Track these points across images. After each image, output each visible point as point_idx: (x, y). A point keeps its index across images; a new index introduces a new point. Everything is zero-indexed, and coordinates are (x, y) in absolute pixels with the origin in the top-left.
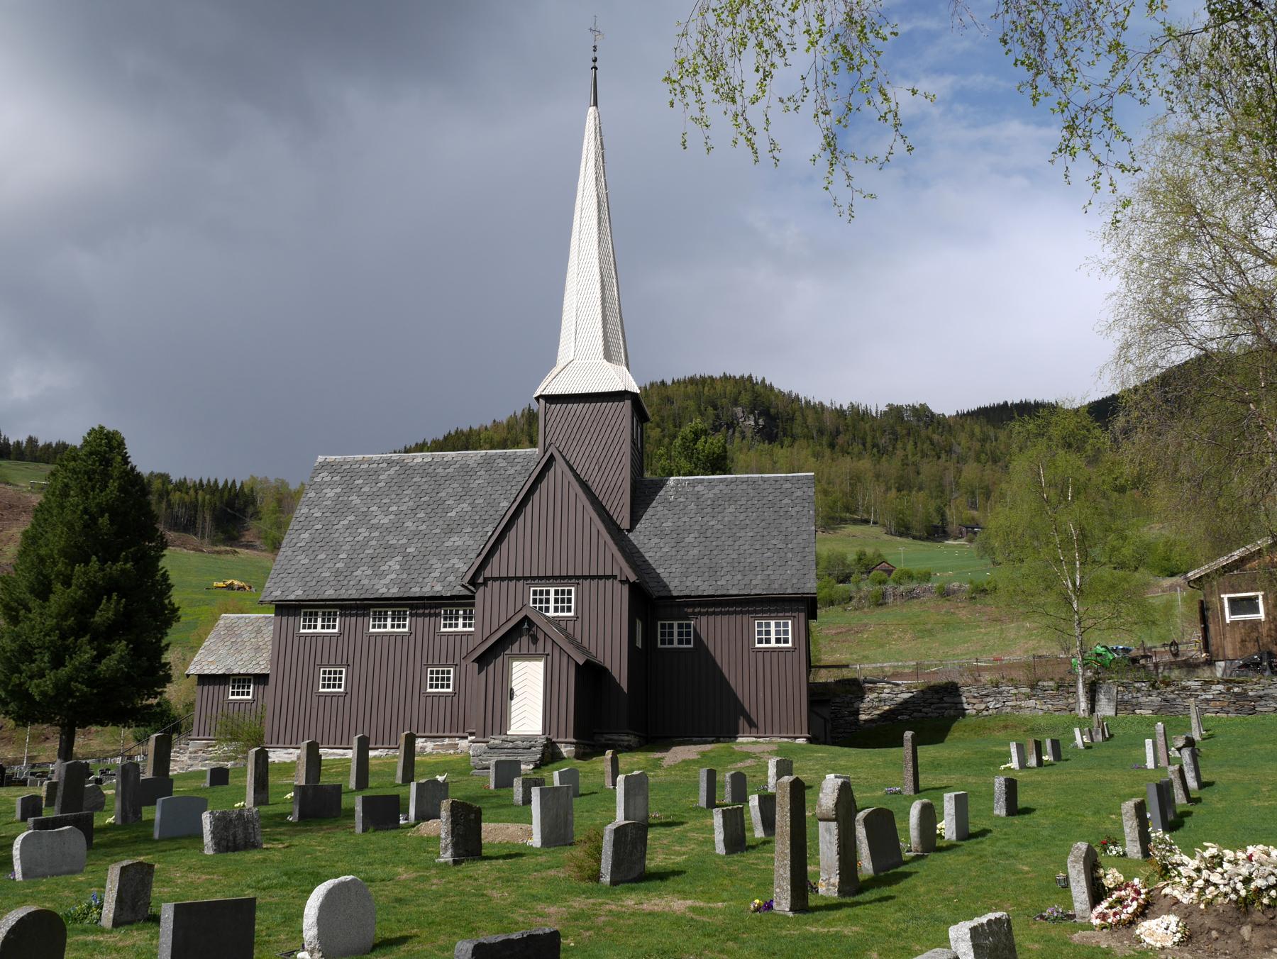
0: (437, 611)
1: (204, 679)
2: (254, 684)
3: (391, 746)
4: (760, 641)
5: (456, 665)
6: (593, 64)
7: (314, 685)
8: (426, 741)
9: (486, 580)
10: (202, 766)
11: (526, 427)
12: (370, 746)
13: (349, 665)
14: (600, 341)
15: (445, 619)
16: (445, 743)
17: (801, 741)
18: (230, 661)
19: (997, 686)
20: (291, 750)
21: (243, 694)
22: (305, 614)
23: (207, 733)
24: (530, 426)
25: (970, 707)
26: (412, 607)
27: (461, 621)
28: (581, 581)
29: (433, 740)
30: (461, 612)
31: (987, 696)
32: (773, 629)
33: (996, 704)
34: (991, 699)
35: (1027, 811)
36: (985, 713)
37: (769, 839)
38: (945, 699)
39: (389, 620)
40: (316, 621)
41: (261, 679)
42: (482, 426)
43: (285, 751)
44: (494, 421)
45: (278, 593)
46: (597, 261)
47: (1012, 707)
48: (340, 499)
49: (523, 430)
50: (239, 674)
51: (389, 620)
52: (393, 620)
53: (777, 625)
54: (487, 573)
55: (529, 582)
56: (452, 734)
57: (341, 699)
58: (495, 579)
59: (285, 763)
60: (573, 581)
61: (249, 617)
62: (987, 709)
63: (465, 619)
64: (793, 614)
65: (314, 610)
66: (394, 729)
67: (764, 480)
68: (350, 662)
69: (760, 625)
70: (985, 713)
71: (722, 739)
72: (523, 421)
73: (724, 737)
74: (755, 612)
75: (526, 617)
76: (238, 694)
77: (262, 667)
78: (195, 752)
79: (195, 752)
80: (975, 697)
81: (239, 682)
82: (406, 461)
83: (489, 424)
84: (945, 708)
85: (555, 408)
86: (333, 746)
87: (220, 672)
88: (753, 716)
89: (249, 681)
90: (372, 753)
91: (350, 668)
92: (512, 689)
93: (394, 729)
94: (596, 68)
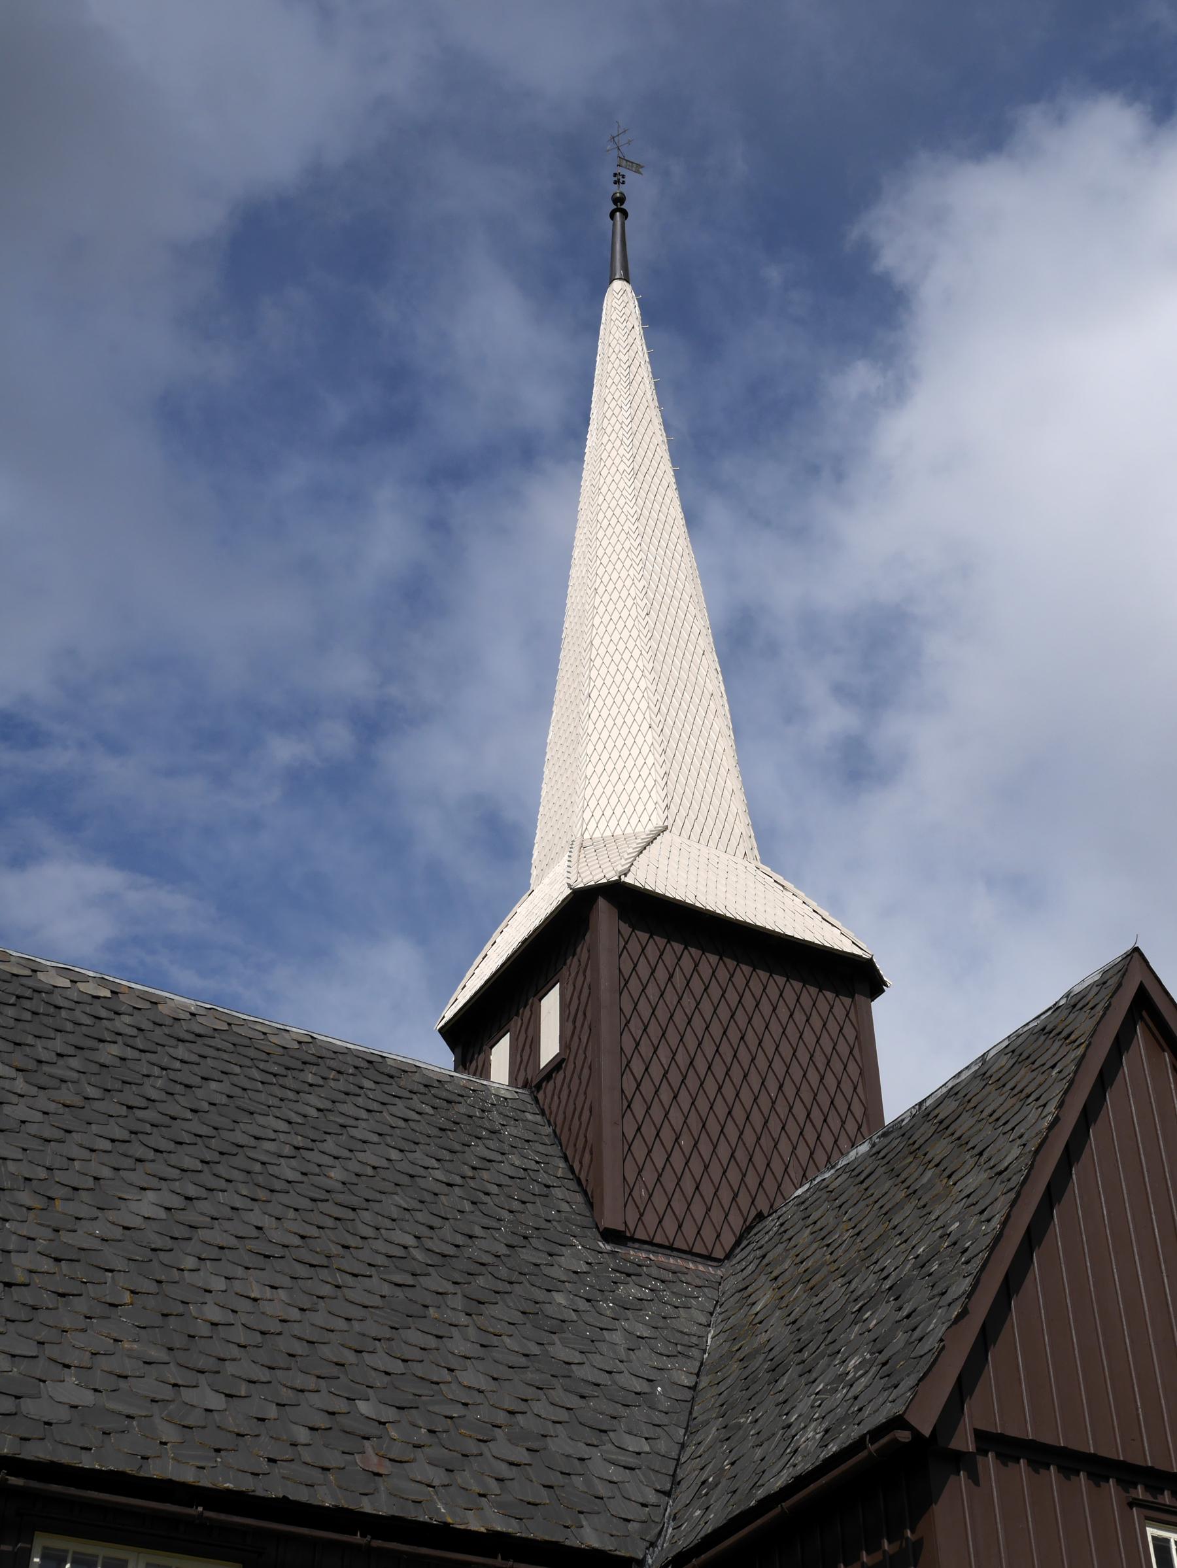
9: (985, 1440)
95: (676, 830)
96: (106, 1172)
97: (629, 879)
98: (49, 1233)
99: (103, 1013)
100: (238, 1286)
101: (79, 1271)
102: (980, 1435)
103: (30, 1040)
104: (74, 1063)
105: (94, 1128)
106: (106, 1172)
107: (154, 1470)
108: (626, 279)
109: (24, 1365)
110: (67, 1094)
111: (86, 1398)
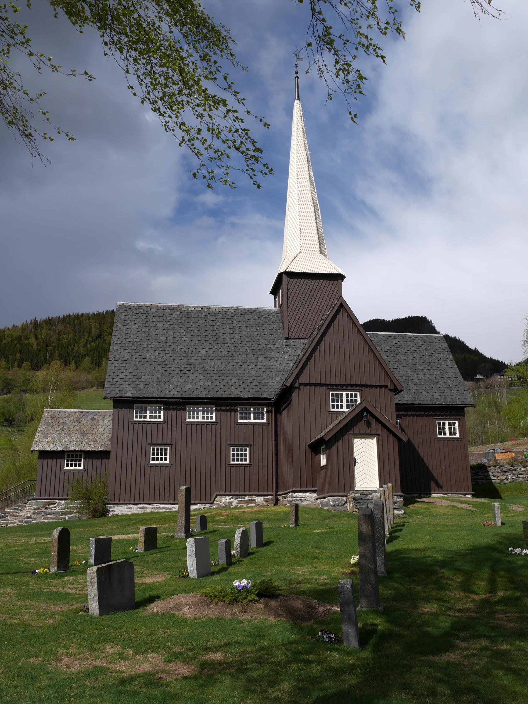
0: (236, 408)
1: (44, 454)
2: (85, 458)
3: (206, 502)
4: (440, 434)
5: (251, 445)
6: (295, 75)
7: (147, 458)
8: (232, 498)
9: (301, 384)
10: (44, 519)
11: (33, 330)
12: (192, 502)
13: (172, 445)
14: (317, 242)
15: (241, 414)
16: (246, 499)
17: (469, 496)
18: (65, 441)
19: (512, 466)
20: (131, 506)
21: (76, 466)
22: (137, 408)
23: (52, 493)
24: (36, 329)
25: (495, 478)
26: (217, 405)
27: (252, 415)
28: (363, 388)
29: (237, 497)
30: (252, 409)
31: (506, 472)
32: (447, 426)
33: (512, 476)
34: (509, 473)
35: (269, 543)
36: (506, 481)
37: (241, 559)
38: (479, 473)
39: (201, 414)
40: (145, 412)
41: (104, 455)
42: (6, 327)
43: (126, 506)
44: (14, 325)
45: (117, 391)
46: (310, 193)
47: (523, 478)
48: (143, 330)
49: (31, 331)
50: (75, 451)
51: (201, 414)
52: (203, 413)
53: (450, 424)
54: (301, 380)
55: (329, 387)
56: (251, 493)
57: (80, 474)
58: (305, 385)
59: (127, 515)
60: (358, 388)
61: (68, 411)
62: (507, 479)
63: (255, 414)
64: (459, 417)
65: (143, 405)
66: (208, 489)
67: (416, 337)
68: (174, 443)
69: (439, 424)
70: (506, 481)
71: (422, 495)
72: (31, 326)
73: (423, 494)
74: (435, 415)
75: (365, 408)
76: (72, 466)
77: (92, 446)
78: (39, 509)
79: (39, 509)
80: (498, 472)
81: (72, 456)
82: (183, 309)
83: (10, 327)
84: (480, 479)
85: (293, 281)
86: (173, 502)
87: (60, 449)
88: (440, 481)
89: (81, 456)
90: (192, 507)
91: (174, 446)
92: (354, 459)
93: (208, 489)
94: (298, 78)
95: (303, 252)
96: (197, 347)
97: (287, 271)
98: (187, 360)
99: (199, 314)
100: (216, 363)
101: (192, 366)
102: (299, 384)
103: (186, 324)
104: (194, 326)
105: (196, 339)
106: (197, 347)
107: (199, 396)
108: (298, 99)
109: (182, 383)
110: (192, 333)
111: (191, 386)
